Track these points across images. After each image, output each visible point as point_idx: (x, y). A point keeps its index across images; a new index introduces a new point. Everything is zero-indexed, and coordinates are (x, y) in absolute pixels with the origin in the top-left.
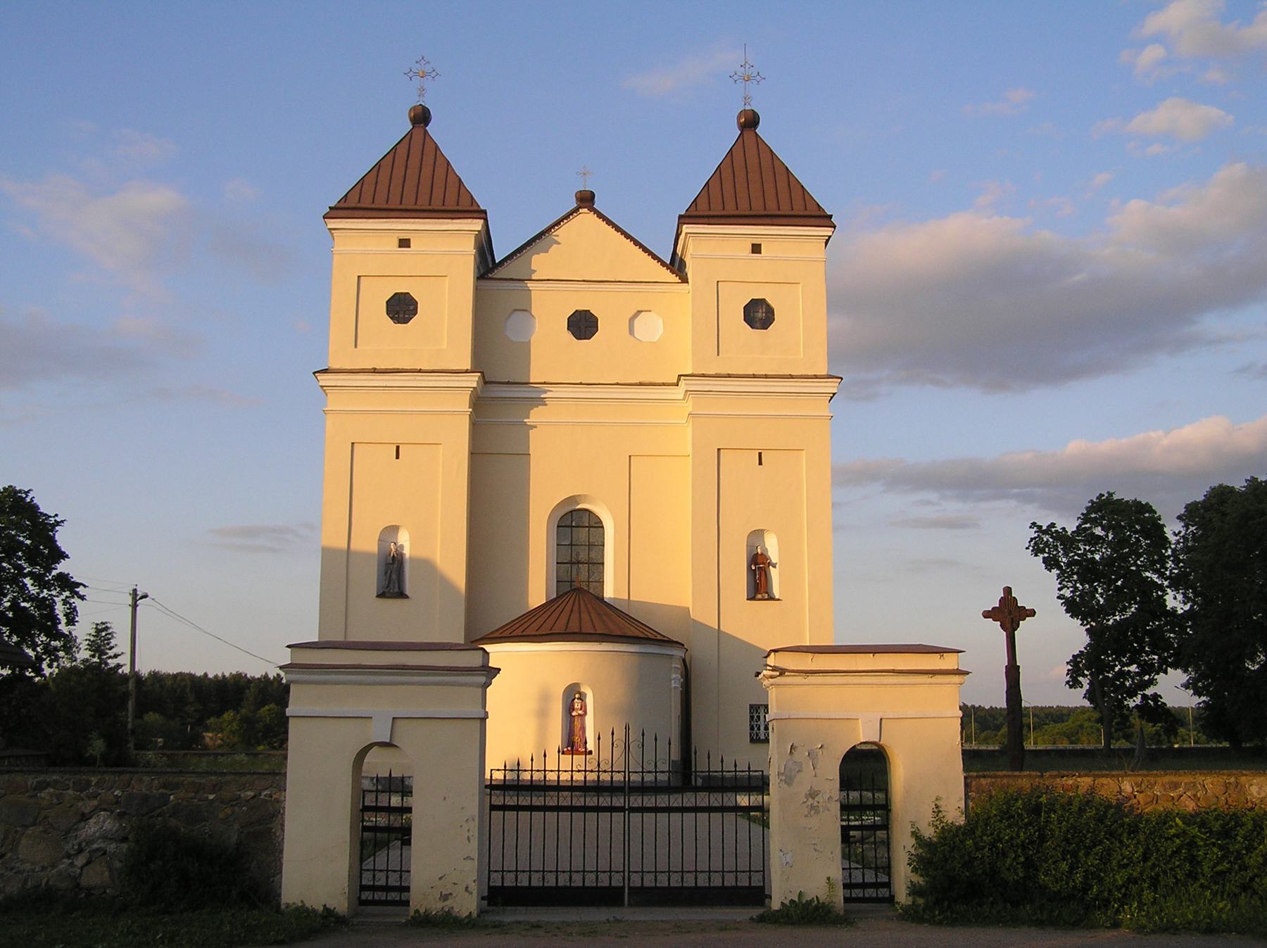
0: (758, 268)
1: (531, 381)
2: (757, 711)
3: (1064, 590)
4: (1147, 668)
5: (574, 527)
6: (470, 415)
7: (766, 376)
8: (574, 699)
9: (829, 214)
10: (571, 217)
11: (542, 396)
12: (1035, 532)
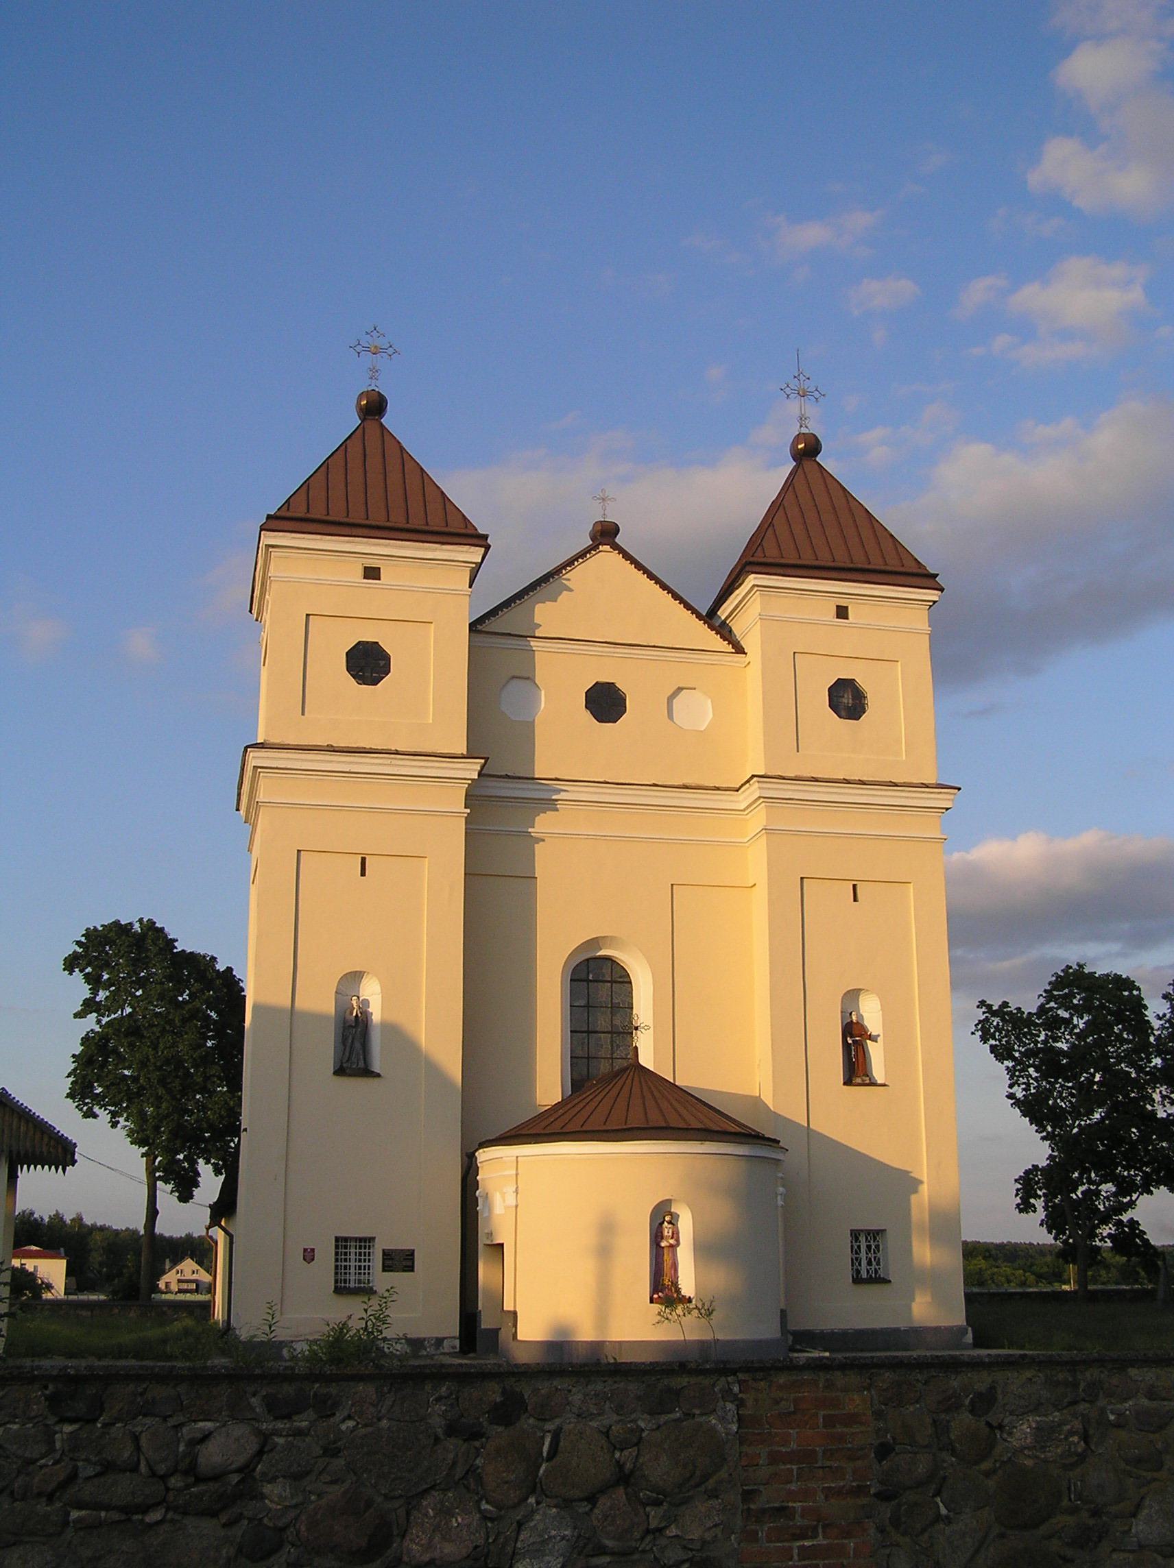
0: (845, 637)
1: (536, 776)
3: (1016, 1087)
4: (1126, 1187)
5: (591, 981)
6: (466, 818)
7: (863, 783)
8: (663, 1223)
9: (932, 572)
10: (588, 556)
11: (554, 797)
12: (984, 1013)
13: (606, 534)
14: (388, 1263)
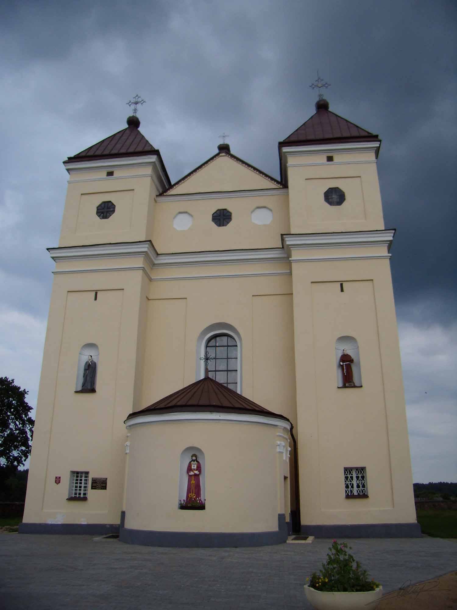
0: (331, 170)
2: (350, 473)
5: (217, 346)
13: (224, 149)
14: (95, 485)
